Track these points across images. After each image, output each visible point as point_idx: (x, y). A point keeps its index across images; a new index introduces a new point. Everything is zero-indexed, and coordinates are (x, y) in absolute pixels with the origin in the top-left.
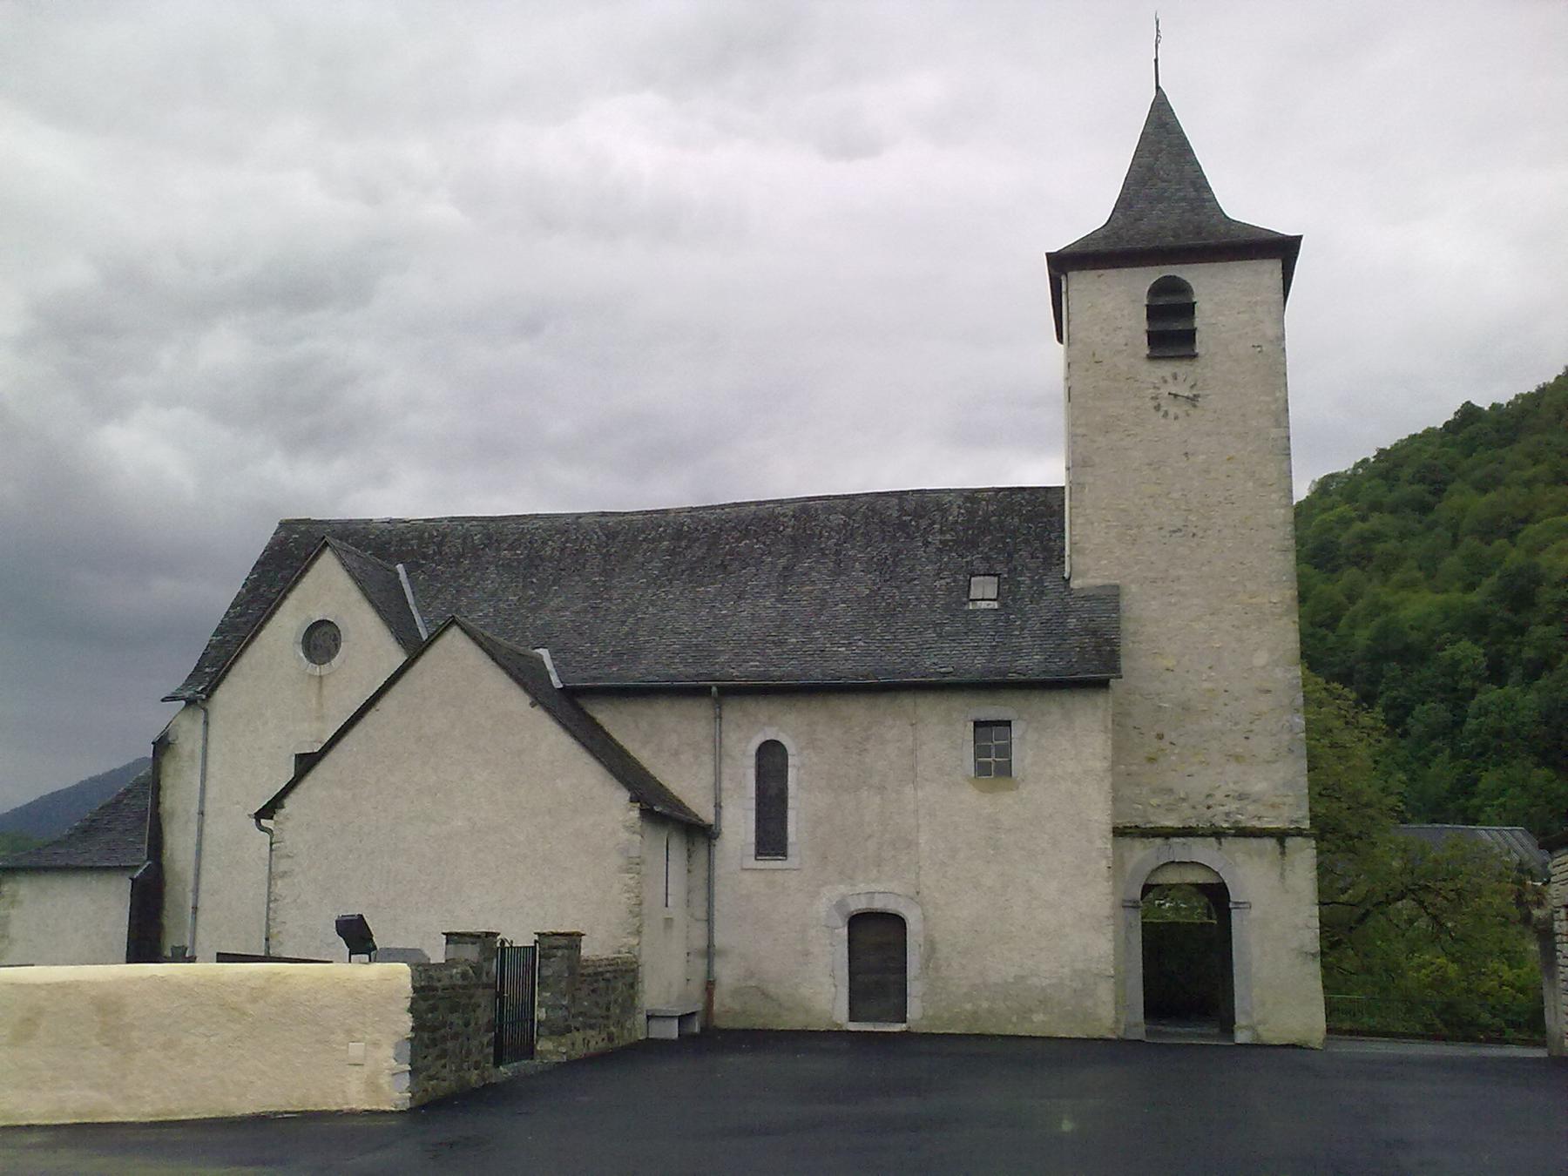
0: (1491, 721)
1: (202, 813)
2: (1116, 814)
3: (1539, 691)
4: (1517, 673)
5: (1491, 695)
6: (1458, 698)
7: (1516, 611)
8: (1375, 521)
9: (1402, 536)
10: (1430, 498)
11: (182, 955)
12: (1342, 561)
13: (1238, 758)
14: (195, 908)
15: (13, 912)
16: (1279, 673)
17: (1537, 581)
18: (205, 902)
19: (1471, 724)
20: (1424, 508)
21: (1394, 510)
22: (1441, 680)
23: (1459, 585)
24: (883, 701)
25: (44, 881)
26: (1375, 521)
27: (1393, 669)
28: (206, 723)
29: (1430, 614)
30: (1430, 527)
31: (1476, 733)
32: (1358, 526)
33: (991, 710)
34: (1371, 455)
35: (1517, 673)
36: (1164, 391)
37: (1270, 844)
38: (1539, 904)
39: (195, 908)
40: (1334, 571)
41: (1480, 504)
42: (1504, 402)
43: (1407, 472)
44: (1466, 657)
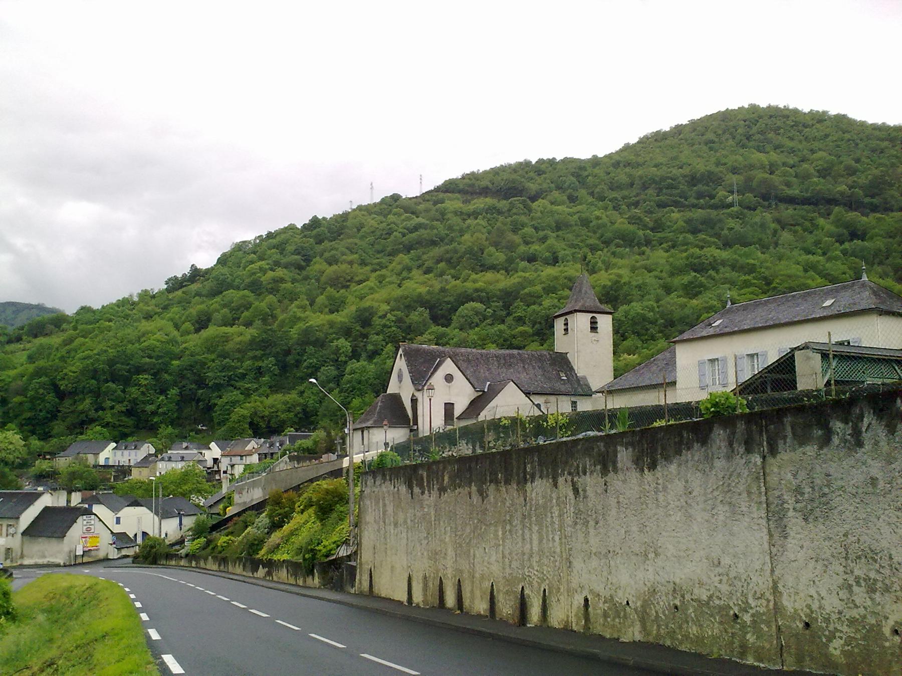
0: (356, 376)
3: (376, 364)
4: (364, 355)
5: (353, 365)
6: (340, 365)
7: (363, 327)
8: (280, 272)
9: (294, 281)
10: (303, 264)
12: (264, 290)
17: (372, 314)
19: (347, 377)
20: (300, 268)
21: (286, 267)
22: (332, 356)
26: (280, 272)
27: (310, 349)
29: (323, 325)
30: (306, 278)
31: (349, 382)
32: (270, 274)
33: (574, 399)
35: (364, 355)
38: (734, 409)
40: (259, 295)
41: (331, 270)
42: (328, 217)
43: (290, 248)
44: (343, 347)
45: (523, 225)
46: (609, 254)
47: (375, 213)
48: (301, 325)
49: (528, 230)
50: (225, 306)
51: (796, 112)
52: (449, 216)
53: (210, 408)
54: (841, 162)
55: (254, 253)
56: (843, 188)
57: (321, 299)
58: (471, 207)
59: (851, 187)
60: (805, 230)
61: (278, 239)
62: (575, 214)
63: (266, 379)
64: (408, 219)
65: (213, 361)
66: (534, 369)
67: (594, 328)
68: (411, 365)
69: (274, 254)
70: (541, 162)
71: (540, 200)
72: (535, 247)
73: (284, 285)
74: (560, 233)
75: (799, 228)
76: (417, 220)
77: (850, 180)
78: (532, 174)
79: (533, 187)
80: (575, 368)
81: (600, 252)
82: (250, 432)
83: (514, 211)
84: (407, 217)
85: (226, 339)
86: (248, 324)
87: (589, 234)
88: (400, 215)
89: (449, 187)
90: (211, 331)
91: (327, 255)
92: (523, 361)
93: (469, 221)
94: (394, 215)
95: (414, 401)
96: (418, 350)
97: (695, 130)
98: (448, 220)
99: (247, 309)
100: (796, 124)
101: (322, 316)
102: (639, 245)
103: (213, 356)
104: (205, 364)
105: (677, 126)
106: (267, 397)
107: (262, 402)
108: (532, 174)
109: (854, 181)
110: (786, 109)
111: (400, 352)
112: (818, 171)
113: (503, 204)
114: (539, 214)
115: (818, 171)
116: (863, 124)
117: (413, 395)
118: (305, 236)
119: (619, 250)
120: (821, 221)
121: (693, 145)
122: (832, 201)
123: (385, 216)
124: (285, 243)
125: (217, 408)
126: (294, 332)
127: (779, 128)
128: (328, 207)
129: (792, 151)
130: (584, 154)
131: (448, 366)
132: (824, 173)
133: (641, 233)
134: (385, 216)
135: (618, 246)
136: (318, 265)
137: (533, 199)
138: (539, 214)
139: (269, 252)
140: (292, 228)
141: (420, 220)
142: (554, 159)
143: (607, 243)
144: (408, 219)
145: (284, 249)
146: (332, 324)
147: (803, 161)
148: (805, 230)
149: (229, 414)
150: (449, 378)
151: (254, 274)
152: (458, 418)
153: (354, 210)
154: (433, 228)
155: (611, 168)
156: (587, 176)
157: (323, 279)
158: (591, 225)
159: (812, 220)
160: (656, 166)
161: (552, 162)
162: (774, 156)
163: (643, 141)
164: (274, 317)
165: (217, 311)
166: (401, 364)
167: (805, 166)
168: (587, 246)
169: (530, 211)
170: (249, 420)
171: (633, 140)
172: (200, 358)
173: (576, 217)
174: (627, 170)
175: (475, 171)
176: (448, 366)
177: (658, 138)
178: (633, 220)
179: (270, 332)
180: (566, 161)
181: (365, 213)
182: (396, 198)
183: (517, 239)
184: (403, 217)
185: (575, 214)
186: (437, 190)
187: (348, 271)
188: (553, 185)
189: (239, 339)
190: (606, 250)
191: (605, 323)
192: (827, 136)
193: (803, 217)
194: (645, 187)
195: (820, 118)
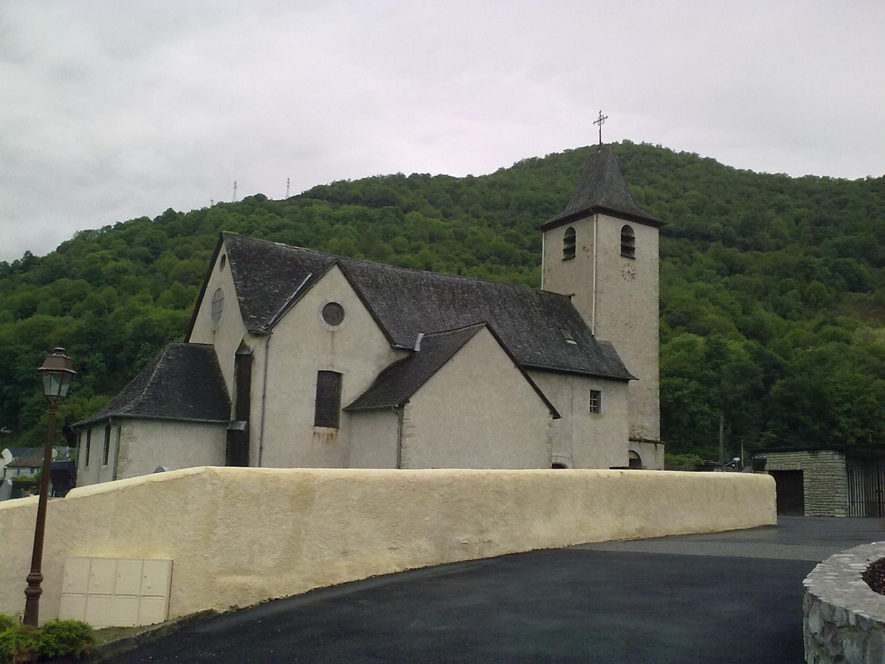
1: (264, 396)
2: (632, 428)
8: (123, 263)
10: (152, 256)
11: (645, 468)
13: (641, 413)
14: (261, 448)
15: (130, 444)
16: (653, 383)
18: (266, 445)
20: (148, 261)
23: (172, 305)
24: (563, 377)
25: (150, 426)
26: (123, 263)
28: (267, 347)
30: (153, 271)
32: (113, 264)
34: (113, 224)
36: (626, 269)
37: (653, 445)
39: (261, 448)
40: (98, 286)
43: (138, 239)
45: (395, 234)
46: (485, 270)
47: (237, 211)
48: (139, 319)
49: (400, 239)
50: (55, 295)
51: (668, 151)
52: (316, 219)
53: (16, 408)
54: (713, 202)
55: (98, 242)
56: (717, 225)
57: (166, 294)
58: (339, 213)
59: (724, 226)
60: (684, 262)
61: (127, 230)
62: (449, 228)
63: (90, 377)
64: (272, 218)
65: (27, 352)
66: (512, 316)
67: (627, 249)
68: (245, 279)
69: (122, 245)
70: (414, 176)
71: (413, 212)
72: (407, 257)
73: (126, 277)
74: (433, 245)
75: (677, 259)
76: (279, 221)
77: (724, 218)
78: (405, 188)
79: (406, 200)
80: (591, 325)
81: (475, 267)
82: (63, 439)
83: (386, 219)
84: (271, 217)
85: (48, 328)
86: (77, 316)
87: (465, 249)
88: (262, 214)
89: (318, 193)
90: (36, 319)
91: (179, 248)
92: (489, 299)
93: (337, 226)
94: (257, 214)
95: (244, 361)
96: (263, 251)
97: (570, 160)
98: (315, 222)
99: (81, 300)
100: (669, 163)
101: (164, 311)
102: (515, 263)
103: (28, 348)
104: (16, 355)
105: (553, 155)
106: (89, 397)
107: (82, 404)
108: (405, 188)
109: (727, 220)
110: (659, 147)
111: (223, 251)
112: (691, 208)
113: (373, 212)
114: (412, 224)
115: (691, 208)
116: (730, 169)
117: (243, 346)
118: (157, 229)
119: (495, 266)
120: (699, 255)
121: (569, 174)
122: (707, 238)
123: (247, 215)
124: (133, 234)
125: (24, 408)
126: (129, 327)
127: (652, 165)
128: (189, 201)
129: (666, 187)
130: (459, 173)
131: (334, 286)
132: (697, 210)
133: (518, 251)
134: (247, 215)
135: (493, 263)
136: (167, 258)
137: (406, 211)
138: (412, 224)
139: (114, 241)
140: (145, 220)
141: (286, 221)
142: (428, 174)
143: (483, 259)
144: (272, 218)
145: (132, 241)
146: (174, 320)
147: (676, 197)
148: (684, 262)
149: (38, 417)
150: (333, 313)
151: (96, 262)
152: (354, 410)
153: (213, 207)
154: (297, 228)
155: (487, 189)
156: (462, 194)
157: (171, 273)
158: (467, 239)
159: (690, 252)
160: (532, 189)
161: (426, 177)
162: (650, 190)
163: (518, 166)
164: (110, 310)
165: (46, 300)
166: (222, 279)
167: (678, 202)
168: (463, 260)
169: (403, 221)
170: (63, 424)
171: (508, 165)
172: (12, 348)
173: (451, 230)
174: (503, 191)
175: (346, 179)
176: (334, 286)
177: (530, 166)
178: (510, 238)
179: (100, 324)
180: (440, 177)
181: (226, 210)
182: (260, 198)
183: (388, 247)
184: (266, 217)
185: (449, 228)
186: (305, 195)
187: (200, 267)
188: (426, 200)
189: (62, 330)
190: (482, 265)
191: (647, 240)
192: (697, 177)
193: (681, 249)
194: (520, 209)
195: (690, 159)
